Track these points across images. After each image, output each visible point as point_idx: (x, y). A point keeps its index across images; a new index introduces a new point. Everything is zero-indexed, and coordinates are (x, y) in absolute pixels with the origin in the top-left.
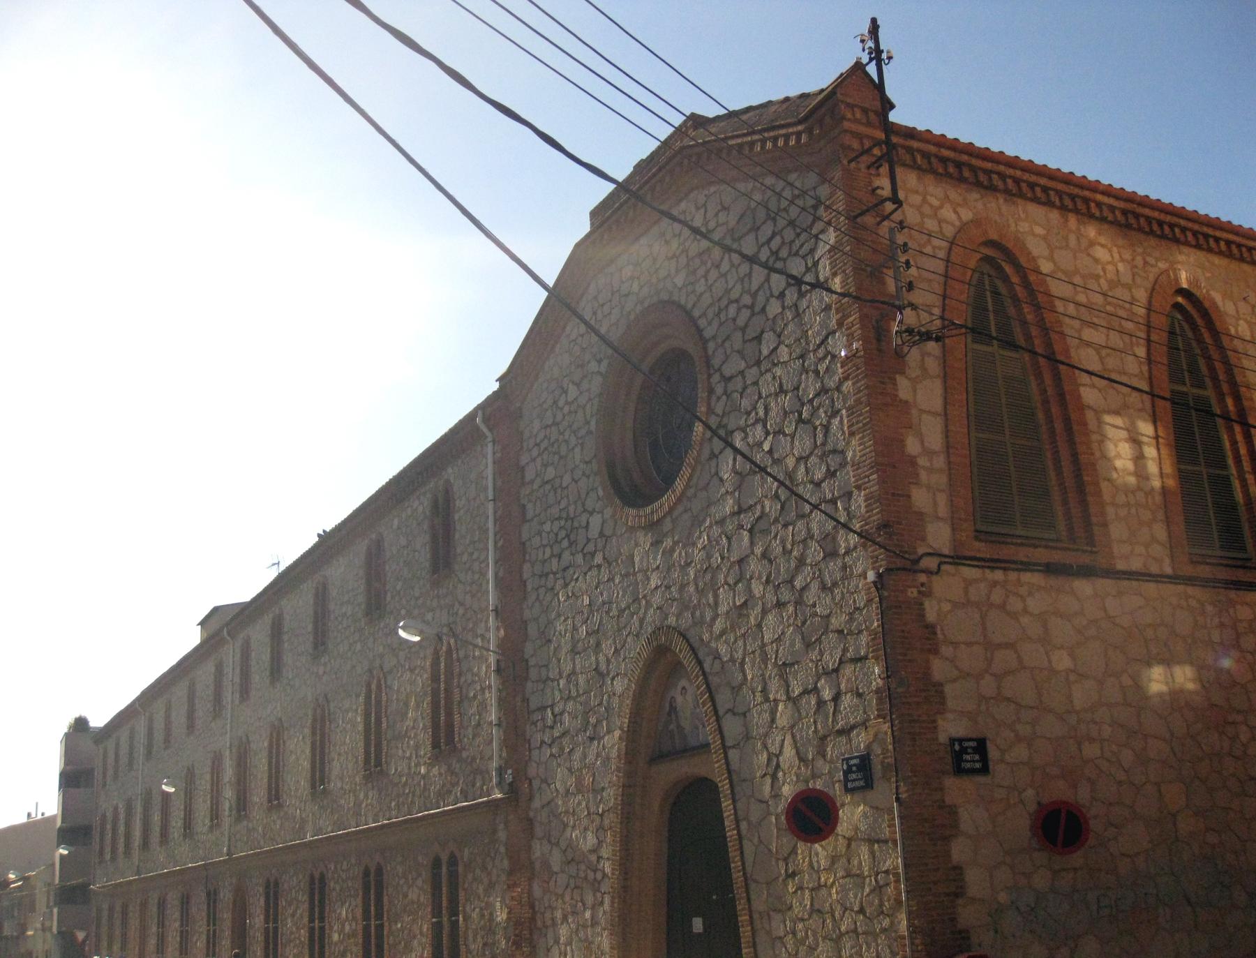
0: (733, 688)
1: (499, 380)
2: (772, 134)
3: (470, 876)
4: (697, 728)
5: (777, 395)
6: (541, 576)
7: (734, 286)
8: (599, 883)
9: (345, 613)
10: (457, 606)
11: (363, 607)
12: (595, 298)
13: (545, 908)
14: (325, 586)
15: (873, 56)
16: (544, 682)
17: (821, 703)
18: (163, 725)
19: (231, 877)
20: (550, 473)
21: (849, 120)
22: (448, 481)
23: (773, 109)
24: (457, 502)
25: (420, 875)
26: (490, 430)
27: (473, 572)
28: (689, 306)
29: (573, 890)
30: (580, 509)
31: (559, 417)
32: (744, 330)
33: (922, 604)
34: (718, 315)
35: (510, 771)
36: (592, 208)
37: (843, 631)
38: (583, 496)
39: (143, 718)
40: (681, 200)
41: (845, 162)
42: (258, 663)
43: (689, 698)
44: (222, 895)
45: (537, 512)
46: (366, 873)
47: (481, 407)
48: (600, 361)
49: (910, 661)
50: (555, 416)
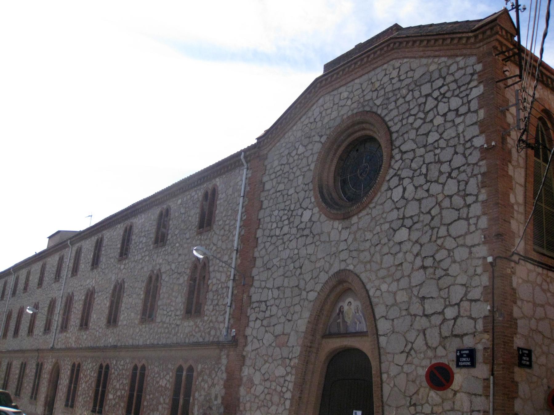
0: (387, 306)
1: (258, 139)
3: (200, 379)
4: (356, 323)
6: (268, 237)
7: (414, 108)
8: (284, 393)
9: (142, 241)
10: (212, 245)
11: (153, 239)
12: (323, 106)
13: (247, 401)
14: (131, 227)
15: (514, 7)
16: (263, 289)
18: (24, 282)
19: (52, 359)
20: (281, 187)
21: (499, 35)
22: (215, 185)
24: (220, 196)
25: (168, 374)
26: (247, 162)
27: (225, 231)
28: (383, 115)
29: (266, 395)
30: (298, 206)
31: (291, 160)
32: (417, 130)
33: (511, 277)
34: (401, 121)
35: (234, 330)
36: (326, 63)
38: (301, 200)
39: (13, 276)
41: (494, 55)
42: (84, 259)
43: (353, 307)
44: (45, 367)
45: (270, 205)
46: (135, 368)
47: (245, 151)
48: (321, 136)
49: (505, 305)
50: (288, 160)
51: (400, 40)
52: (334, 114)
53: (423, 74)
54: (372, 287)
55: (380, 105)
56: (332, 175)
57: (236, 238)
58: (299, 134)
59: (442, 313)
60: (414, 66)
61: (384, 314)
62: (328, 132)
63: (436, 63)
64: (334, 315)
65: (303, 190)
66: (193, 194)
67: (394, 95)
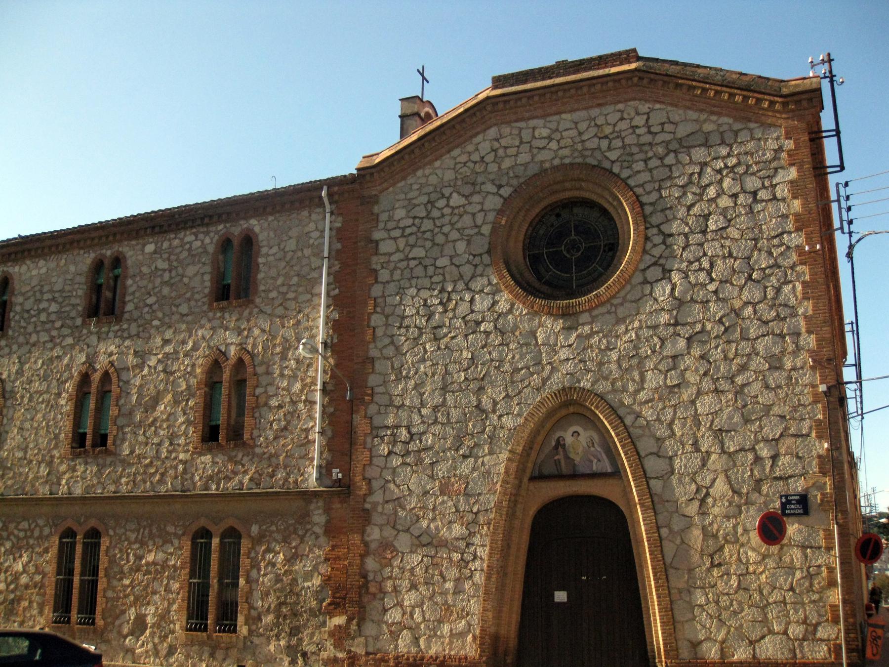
2: (772, 98)
4: (592, 462)
5: (724, 257)
11: (80, 308)
17: (758, 459)
20: (419, 252)
23: (747, 79)
37: (784, 417)
40: (619, 102)
51: (652, 76)
52: (524, 158)
53: (693, 133)
54: (629, 413)
55: (617, 160)
56: (520, 245)
57: (321, 322)
58: (449, 175)
59: (404, 464)
60: (676, 118)
61: (655, 450)
62: (515, 182)
63: (714, 122)
64: (547, 450)
65: (468, 262)
66: (188, 239)
67: (641, 151)
